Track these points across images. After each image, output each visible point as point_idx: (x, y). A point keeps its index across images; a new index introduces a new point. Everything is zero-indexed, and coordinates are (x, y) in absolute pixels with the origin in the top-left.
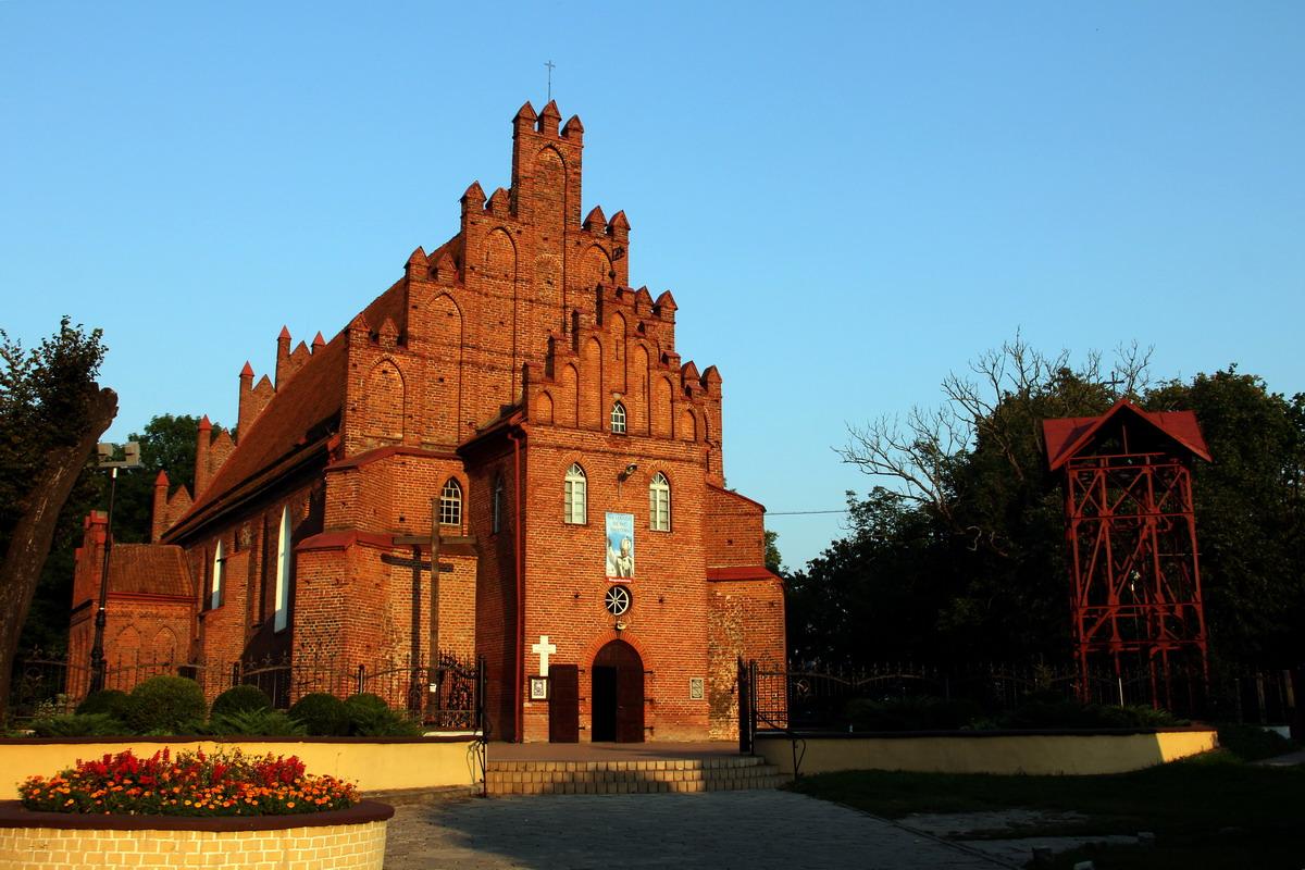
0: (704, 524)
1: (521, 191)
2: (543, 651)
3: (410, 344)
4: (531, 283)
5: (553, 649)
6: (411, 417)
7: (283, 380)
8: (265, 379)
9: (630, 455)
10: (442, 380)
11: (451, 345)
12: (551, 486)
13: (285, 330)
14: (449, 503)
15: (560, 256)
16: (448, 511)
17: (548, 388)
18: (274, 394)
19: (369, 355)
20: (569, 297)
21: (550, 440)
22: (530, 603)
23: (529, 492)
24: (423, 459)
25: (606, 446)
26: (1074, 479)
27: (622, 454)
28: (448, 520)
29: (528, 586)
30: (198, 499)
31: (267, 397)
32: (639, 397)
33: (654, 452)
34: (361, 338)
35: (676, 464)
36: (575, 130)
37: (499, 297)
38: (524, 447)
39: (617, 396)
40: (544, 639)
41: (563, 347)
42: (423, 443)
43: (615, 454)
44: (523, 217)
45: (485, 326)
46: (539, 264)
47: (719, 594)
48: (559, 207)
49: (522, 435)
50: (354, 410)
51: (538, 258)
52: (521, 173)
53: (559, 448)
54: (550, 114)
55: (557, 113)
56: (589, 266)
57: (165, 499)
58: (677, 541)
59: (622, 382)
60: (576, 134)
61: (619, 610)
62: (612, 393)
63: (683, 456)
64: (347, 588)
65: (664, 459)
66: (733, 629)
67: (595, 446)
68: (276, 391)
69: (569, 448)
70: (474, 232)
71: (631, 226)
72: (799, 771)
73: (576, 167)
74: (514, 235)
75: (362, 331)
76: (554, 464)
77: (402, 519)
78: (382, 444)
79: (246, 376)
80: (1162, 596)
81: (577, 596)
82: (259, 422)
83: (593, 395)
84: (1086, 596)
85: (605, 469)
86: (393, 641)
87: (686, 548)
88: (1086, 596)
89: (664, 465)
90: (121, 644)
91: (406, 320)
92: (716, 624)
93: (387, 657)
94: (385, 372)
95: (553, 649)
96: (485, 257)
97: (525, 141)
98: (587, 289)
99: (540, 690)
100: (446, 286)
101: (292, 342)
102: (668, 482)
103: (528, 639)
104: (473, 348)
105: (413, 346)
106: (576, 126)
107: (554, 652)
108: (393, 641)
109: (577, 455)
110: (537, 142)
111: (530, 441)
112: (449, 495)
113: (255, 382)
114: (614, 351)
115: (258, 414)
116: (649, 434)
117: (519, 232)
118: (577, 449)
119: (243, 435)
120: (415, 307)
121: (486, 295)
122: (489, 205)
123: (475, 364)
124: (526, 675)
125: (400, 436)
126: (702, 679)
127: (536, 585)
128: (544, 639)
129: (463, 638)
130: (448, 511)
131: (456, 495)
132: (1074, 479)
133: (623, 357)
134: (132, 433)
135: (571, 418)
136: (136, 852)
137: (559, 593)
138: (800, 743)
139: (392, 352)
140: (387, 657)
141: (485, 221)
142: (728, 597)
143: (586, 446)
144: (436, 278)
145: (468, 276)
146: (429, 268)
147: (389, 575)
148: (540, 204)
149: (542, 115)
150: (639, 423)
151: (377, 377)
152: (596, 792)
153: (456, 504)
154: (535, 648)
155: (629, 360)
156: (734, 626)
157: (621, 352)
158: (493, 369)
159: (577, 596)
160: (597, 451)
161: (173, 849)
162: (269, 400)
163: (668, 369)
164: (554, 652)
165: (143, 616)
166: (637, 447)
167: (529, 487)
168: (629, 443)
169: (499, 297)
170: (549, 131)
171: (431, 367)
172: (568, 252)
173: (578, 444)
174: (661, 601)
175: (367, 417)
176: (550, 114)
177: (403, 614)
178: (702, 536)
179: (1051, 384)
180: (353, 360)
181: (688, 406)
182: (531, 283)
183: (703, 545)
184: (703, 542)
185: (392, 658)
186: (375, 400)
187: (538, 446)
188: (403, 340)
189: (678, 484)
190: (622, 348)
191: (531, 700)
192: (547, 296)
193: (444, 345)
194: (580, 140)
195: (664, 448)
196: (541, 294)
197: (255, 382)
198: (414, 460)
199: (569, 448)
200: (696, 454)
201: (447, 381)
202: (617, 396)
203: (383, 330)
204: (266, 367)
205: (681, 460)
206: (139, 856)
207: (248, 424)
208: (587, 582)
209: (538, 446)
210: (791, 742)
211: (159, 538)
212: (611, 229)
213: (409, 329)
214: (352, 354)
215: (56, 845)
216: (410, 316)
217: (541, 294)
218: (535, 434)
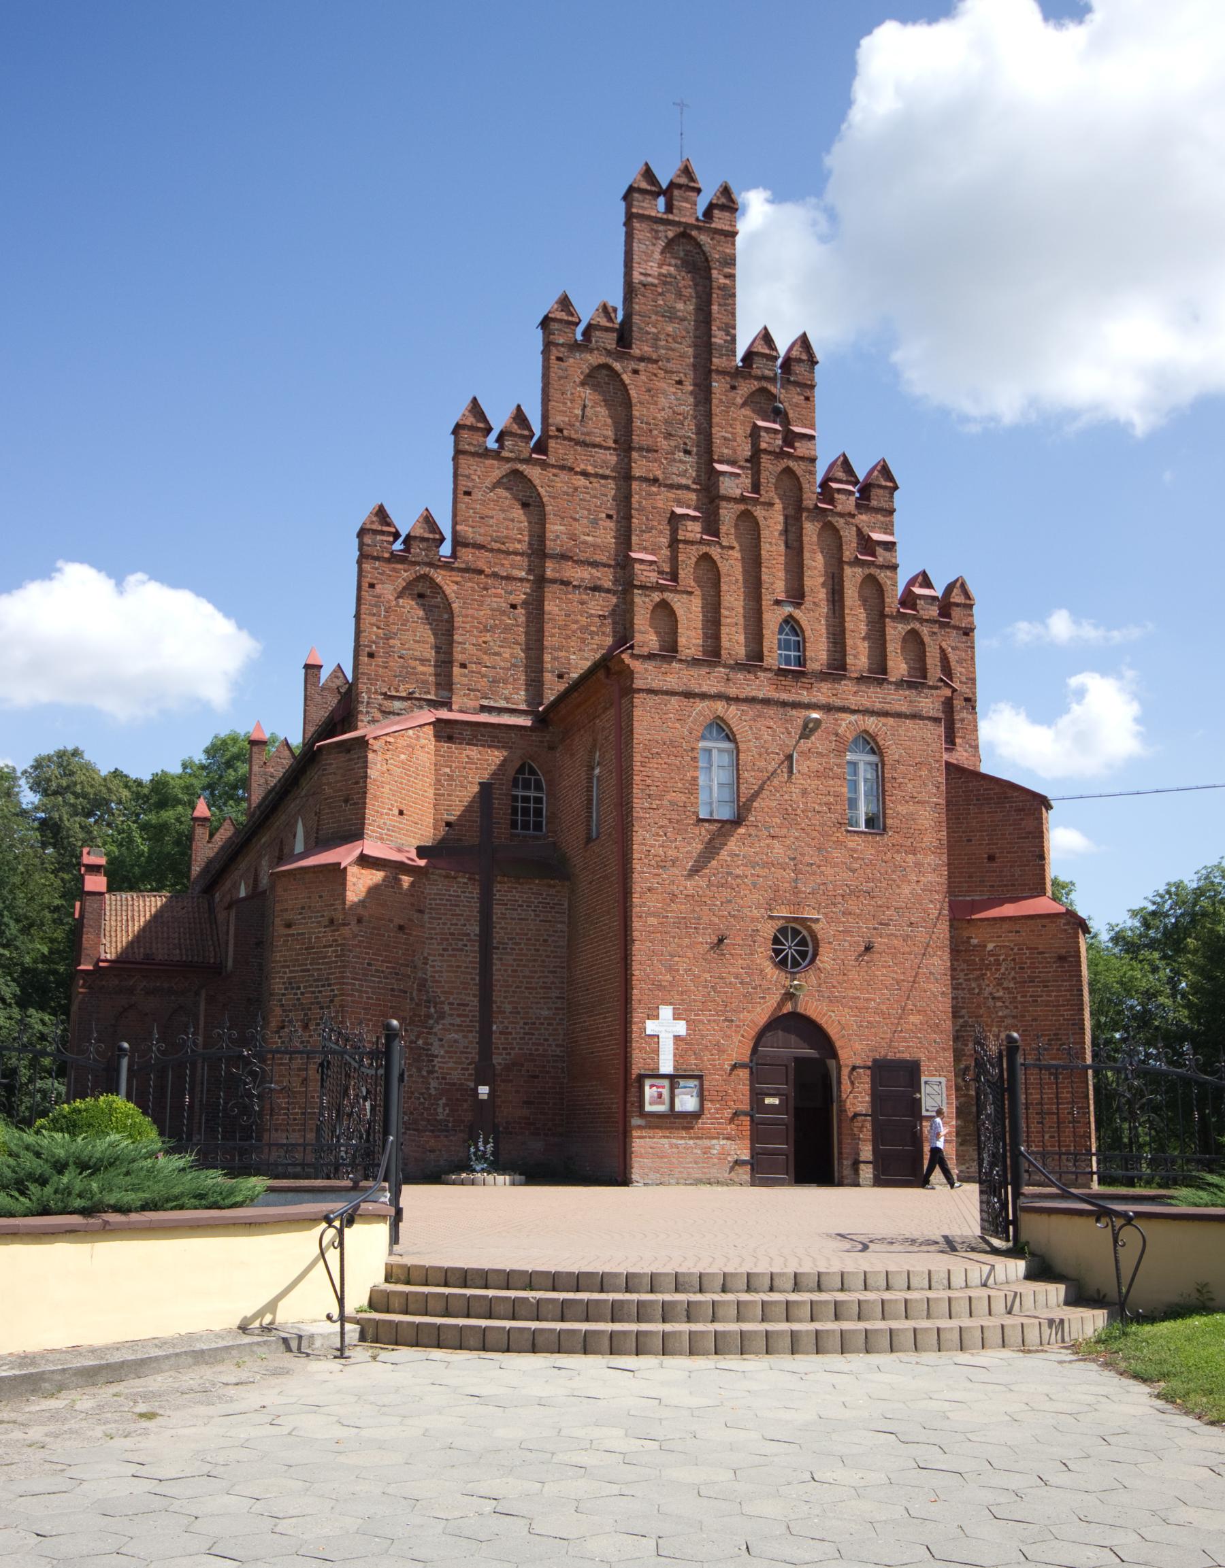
5: (681, 1028)
6: (463, 666)
14: (526, 799)
16: (526, 811)
17: (668, 596)
19: (394, 570)
27: (796, 705)
28: (526, 826)
29: (636, 924)
40: (666, 1012)
43: (784, 704)
47: (974, 941)
52: (637, 278)
53: (688, 695)
54: (687, 182)
64: (346, 931)
66: (999, 998)
70: (561, 373)
86: (429, 1016)
87: (910, 859)
89: (871, 723)
92: (971, 990)
93: (420, 1042)
95: (681, 1028)
108: (429, 1016)
112: (526, 786)
116: (837, 668)
122: (587, 333)
124: (635, 1072)
126: (943, 1080)
128: (666, 1012)
129: (545, 1013)
130: (526, 811)
131: (538, 787)
137: (690, 936)
140: (420, 1042)
142: (990, 946)
147: (421, 911)
148: (670, 329)
149: (672, 185)
150: (818, 653)
152: (300, 1337)
153: (538, 800)
154: (651, 1027)
156: (1001, 994)
170: (680, 209)
176: (687, 182)
177: (445, 974)
179: (1202, 1359)
185: (426, 1043)
200: (929, 703)
205: (899, 715)
212: (866, 490)
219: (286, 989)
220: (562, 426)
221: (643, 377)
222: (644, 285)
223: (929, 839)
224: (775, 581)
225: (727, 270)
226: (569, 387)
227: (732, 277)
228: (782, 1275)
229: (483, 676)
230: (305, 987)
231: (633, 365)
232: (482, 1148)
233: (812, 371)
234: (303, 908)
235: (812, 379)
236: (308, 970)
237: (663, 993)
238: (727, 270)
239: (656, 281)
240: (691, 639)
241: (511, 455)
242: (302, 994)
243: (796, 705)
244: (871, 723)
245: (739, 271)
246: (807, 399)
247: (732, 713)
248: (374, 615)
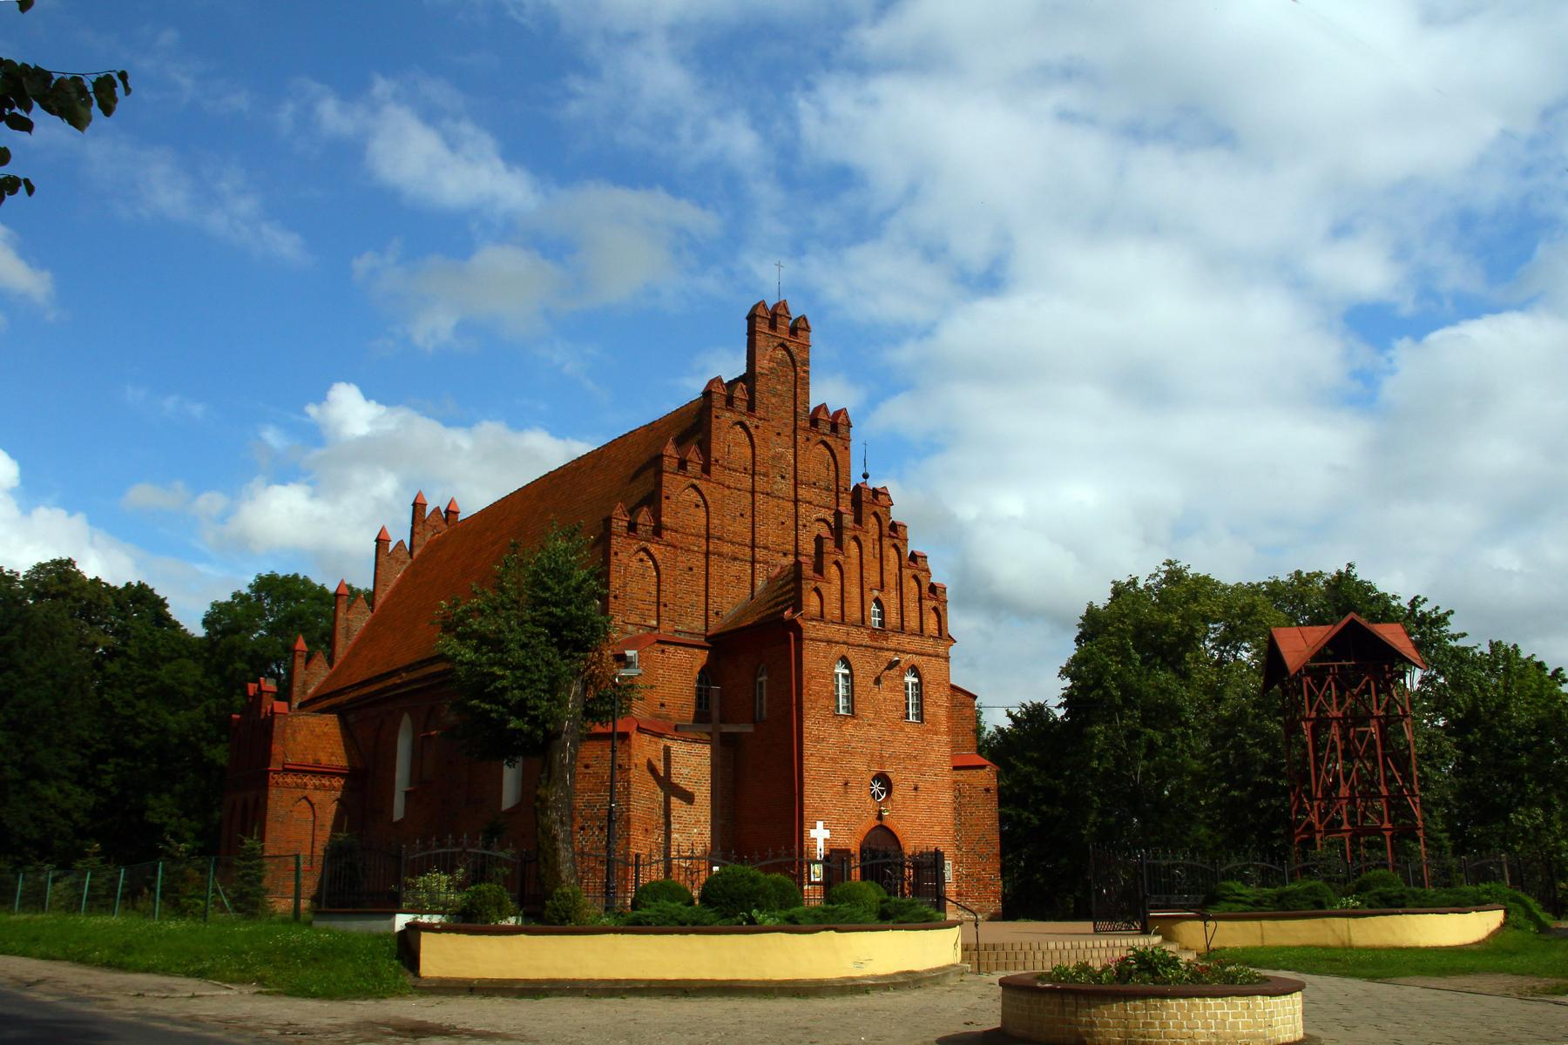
0: (950, 718)
1: (757, 387)
2: (819, 835)
3: (665, 533)
4: (768, 476)
5: (827, 834)
6: (665, 606)
7: (419, 546)
8: (401, 543)
9: (888, 650)
10: (691, 569)
11: (698, 536)
12: (823, 679)
13: (419, 495)
15: (791, 451)
18: (409, 561)
19: (629, 544)
20: (800, 491)
21: (821, 634)
22: (807, 790)
23: (805, 683)
24: (681, 648)
25: (867, 641)
26: (1307, 683)
27: (881, 649)
29: (805, 774)
30: (336, 665)
31: (404, 563)
32: (893, 594)
33: (908, 647)
34: (622, 526)
35: (925, 658)
36: (803, 329)
37: (739, 490)
38: (799, 639)
39: (876, 593)
40: (820, 824)
41: (829, 545)
42: (676, 631)
43: (876, 648)
44: (760, 412)
45: (728, 517)
46: (773, 458)
48: (790, 404)
49: (798, 630)
50: (616, 597)
51: (772, 452)
53: (829, 642)
55: (788, 313)
56: (814, 460)
57: (304, 664)
58: (928, 731)
59: (879, 579)
60: (804, 333)
61: (879, 797)
62: (871, 589)
63: (931, 650)
65: (916, 654)
67: (858, 641)
68: (411, 553)
69: (837, 643)
71: (853, 424)
72: (1211, 946)
73: (805, 365)
74: (752, 431)
75: (622, 520)
76: (824, 657)
77: (662, 705)
78: (641, 631)
79: (381, 542)
80: (1385, 788)
81: (846, 784)
82: (398, 586)
83: (853, 591)
84: (1320, 789)
85: (868, 662)
88: (1320, 789)
89: (916, 660)
90: (295, 815)
91: (660, 510)
94: (641, 560)
95: (827, 834)
96: (726, 450)
97: (760, 341)
98: (815, 484)
99: (817, 872)
100: (695, 478)
101: (427, 506)
102: (848, 666)
103: (807, 825)
104: (719, 539)
105: (667, 535)
106: (804, 325)
107: (828, 836)
109: (844, 649)
110: (771, 340)
111: (805, 635)
113: (392, 546)
114: (871, 550)
115: (394, 581)
116: (902, 629)
117: (757, 427)
118: (845, 643)
119: (380, 599)
120: (667, 498)
121: (728, 487)
123: (720, 555)
125: (654, 623)
127: (813, 773)
132: (1307, 683)
133: (878, 556)
134: (235, 590)
135: (857, 615)
136: (1226, 1011)
138: (1211, 924)
139: (648, 541)
141: (728, 414)
143: (851, 640)
144: (685, 469)
145: (713, 468)
146: (679, 459)
148: (773, 400)
150: (893, 618)
151: (635, 564)
154: (813, 833)
155: (885, 558)
157: (877, 551)
158: (735, 559)
159: (846, 784)
160: (861, 646)
161: (1248, 1008)
162: (405, 567)
163: (917, 568)
164: (828, 836)
165: (316, 788)
166: (893, 642)
167: (805, 679)
168: (886, 639)
169: (739, 490)
170: (781, 329)
171: (682, 557)
172: (799, 447)
173: (844, 638)
174: (916, 789)
175: (627, 604)
178: (948, 727)
180: (614, 549)
181: (933, 604)
182: (768, 476)
183: (949, 735)
184: (950, 732)
186: (633, 587)
187: (812, 640)
188: (658, 530)
189: (927, 677)
190: (877, 547)
191: (810, 883)
192: (781, 489)
193: (692, 535)
194: (807, 338)
195: (915, 643)
196: (775, 487)
197: (392, 546)
198: (672, 649)
199: (837, 643)
201: (695, 570)
202: (876, 593)
203: (640, 520)
204: (400, 533)
205: (929, 655)
206: (1228, 1013)
207: (384, 590)
208: (854, 770)
209: (812, 640)
210: (1092, 923)
211: (297, 704)
213: (663, 519)
214: (613, 541)
215: (1167, 1007)
216: (664, 506)
217: (775, 487)
218: (810, 629)
219: (585, 806)
220: (718, 457)
221: (760, 430)
222: (762, 374)
223: (943, 728)
224: (872, 577)
225: (805, 368)
226: (1454, 875)
227: (807, 372)
228: (1007, 944)
229: (676, 611)
230: (600, 806)
231: (756, 421)
232: (1362, 840)
233: (848, 431)
234: (597, 757)
235: (849, 437)
236: (602, 796)
237: (820, 813)
238: (805, 368)
239: (767, 372)
240: (833, 609)
241: (691, 475)
242: (598, 810)
243: (881, 649)
244: (916, 660)
245: (811, 369)
246: (846, 448)
247: (851, 654)
248: (617, 571)
